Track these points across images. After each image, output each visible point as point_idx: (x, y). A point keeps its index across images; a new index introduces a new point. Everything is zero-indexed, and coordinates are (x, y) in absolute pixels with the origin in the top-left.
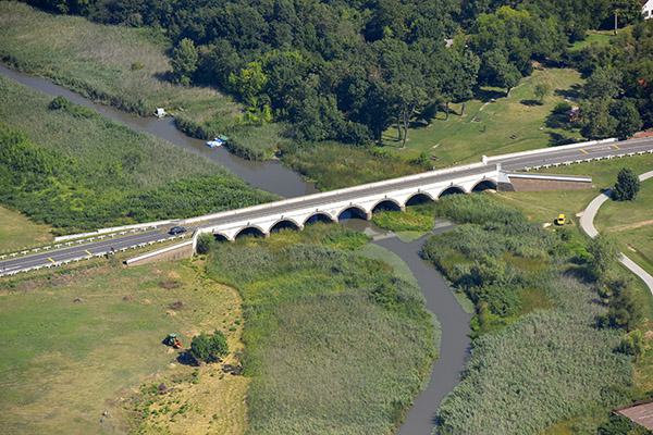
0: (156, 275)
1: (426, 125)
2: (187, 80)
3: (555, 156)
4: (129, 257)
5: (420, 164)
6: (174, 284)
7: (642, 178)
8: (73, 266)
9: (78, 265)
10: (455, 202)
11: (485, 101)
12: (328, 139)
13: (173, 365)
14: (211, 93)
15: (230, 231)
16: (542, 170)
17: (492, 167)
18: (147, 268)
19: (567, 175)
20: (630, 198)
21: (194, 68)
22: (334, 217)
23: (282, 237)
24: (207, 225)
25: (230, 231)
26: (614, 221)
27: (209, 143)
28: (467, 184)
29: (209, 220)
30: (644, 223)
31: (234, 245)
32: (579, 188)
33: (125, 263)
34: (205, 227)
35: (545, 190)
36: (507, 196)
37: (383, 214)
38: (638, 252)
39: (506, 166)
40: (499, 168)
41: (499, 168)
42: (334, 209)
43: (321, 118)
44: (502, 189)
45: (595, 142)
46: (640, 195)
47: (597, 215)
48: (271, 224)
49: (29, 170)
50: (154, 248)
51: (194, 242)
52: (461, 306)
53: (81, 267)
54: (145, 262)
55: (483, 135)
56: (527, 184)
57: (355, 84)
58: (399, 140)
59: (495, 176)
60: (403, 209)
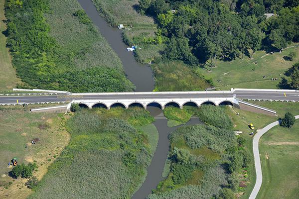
0: (41, 120)
1: (231, 60)
2: (143, 11)
3: (269, 94)
4: (34, 108)
5: (209, 84)
6: (46, 126)
7: (297, 117)
8: (6, 107)
9: (8, 107)
10: (208, 113)
11: (267, 53)
12: (179, 59)
13: (4, 175)
14: (151, 20)
15: (90, 103)
16: (256, 102)
17: (231, 95)
18: (38, 115)
19: (268, 107)
20: (288, 126)
21: (147, 7)
22: (145, 106)
23: (117, 112)
24: (78, 98)
25: (90, 103)
26: (271, 138)
27: (128, 48)
28: (217, 101)
29: (84, 96)
30: (284, 143)
31: (92, 110)
32: (269, 115)
33: (31, 110)
34: (76, 99)
35: (252, 113)
36: (235, 111)
37: (171, 108)
38: (268, 161)
39: (238, 95)
40: (234, 97)
41: (234, 97)
42: (145, 102)
43: (177, 49)
44: (235, 106)
45: (294, 91)
46: (295, 125)
47: (267, 132)
48: (93, 104)
49: (37, 47)
50: (48, 106)
51: (69, 106)
52: (163, 172)
53: (9, 109)
54: (41, 112)
55: (252, 73)
56: (246, 107)
57: (200, 35)
58: (214, 68)
59: (232, 100)
60: (163, 108)
